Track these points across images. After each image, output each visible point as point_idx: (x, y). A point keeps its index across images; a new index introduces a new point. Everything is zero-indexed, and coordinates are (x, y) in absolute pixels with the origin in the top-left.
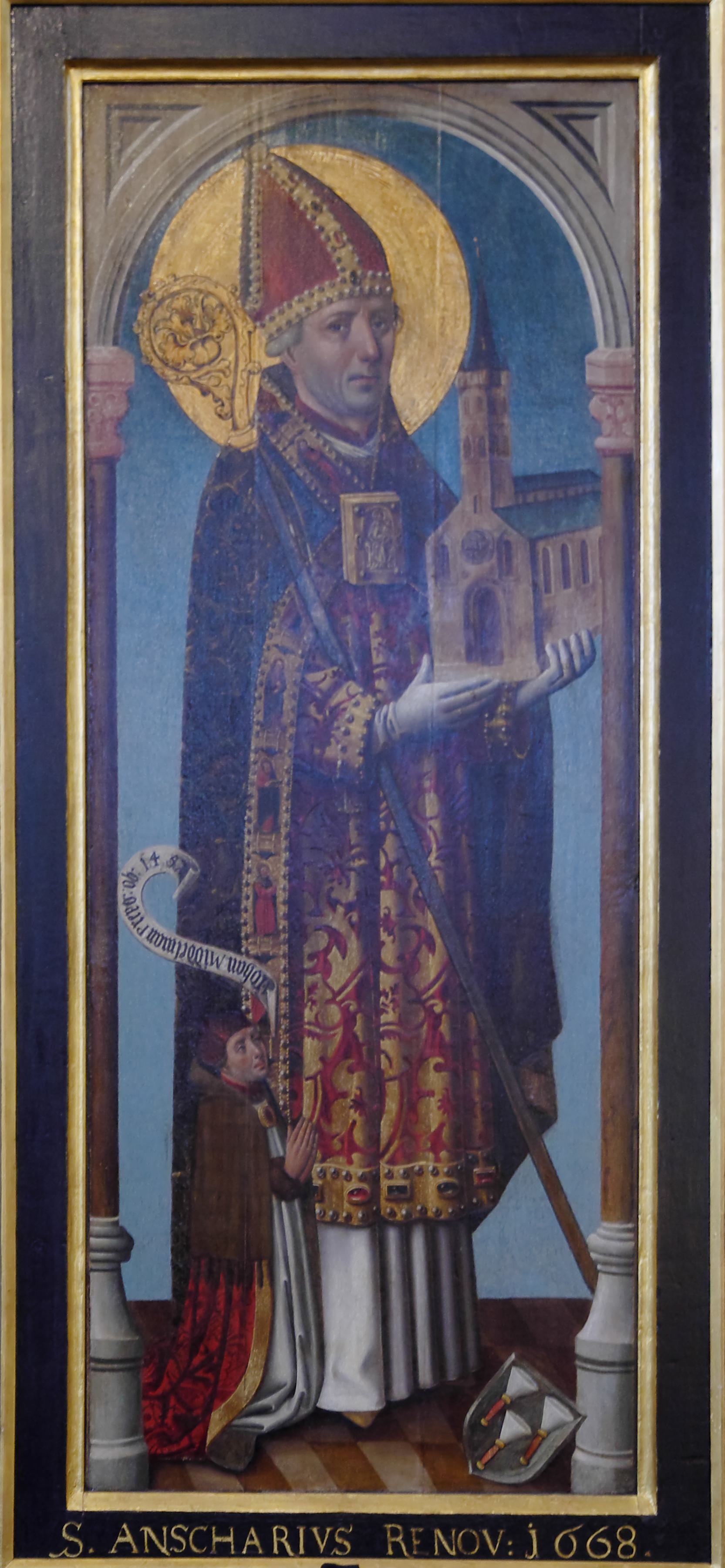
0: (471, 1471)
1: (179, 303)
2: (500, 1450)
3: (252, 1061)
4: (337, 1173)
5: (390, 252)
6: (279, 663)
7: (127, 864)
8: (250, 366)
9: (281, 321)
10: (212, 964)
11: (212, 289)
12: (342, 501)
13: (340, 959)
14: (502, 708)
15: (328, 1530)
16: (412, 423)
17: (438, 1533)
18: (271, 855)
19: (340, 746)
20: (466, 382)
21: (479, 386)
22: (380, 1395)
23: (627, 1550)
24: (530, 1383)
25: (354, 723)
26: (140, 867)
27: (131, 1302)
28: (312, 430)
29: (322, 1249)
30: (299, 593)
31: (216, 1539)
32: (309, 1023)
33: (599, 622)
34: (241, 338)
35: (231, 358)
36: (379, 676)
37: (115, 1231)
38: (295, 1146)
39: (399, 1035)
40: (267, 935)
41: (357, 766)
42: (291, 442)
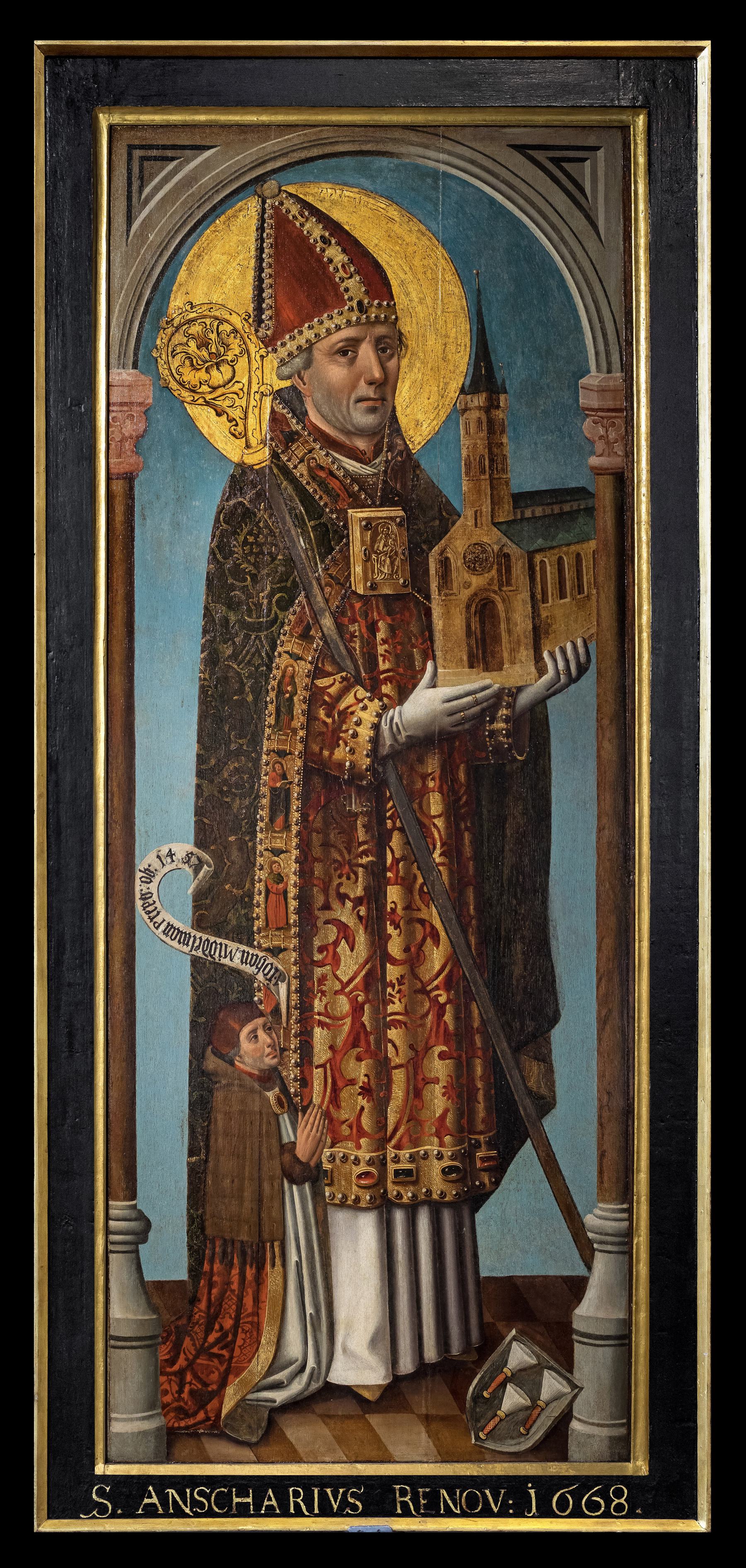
0: (473, 1441)
1: (196, 329)
2: (501, 1420)
3: (264, 1050)
4: (345, 1158)
5: (394, 283)
6: (291, 669)
7: (145, 859)
8: (262, 389)
9: (291, 346)
10: (226, 957)
11: (227, 316)
12: (349, 515)
13: (348, 952)
14: (503, 712)
15: (341, 1490)
16: (416, 443)
17: (443, 1492)
18: (283, 852)
19: (348, 749)
20: (466, 404)
21: (479, 408)
22: (387, 1370)
23: (620, 1507)
24: (530, 1357)
25: (361, 726)
26: (156, 864)
27: (148, 1282)
28: (321, 449)
29: (332, 1230)
30: (309, 603)
31: (236, 1500)
32: (319, 1014)
33: (593, 630)
34: (254, 362)
35: (245, 380)
37: (134, 1214)
38: (306, 1132)
39: (405, 1024)
40: (278, 929)
41: (364, 767)
42: (302, 461)
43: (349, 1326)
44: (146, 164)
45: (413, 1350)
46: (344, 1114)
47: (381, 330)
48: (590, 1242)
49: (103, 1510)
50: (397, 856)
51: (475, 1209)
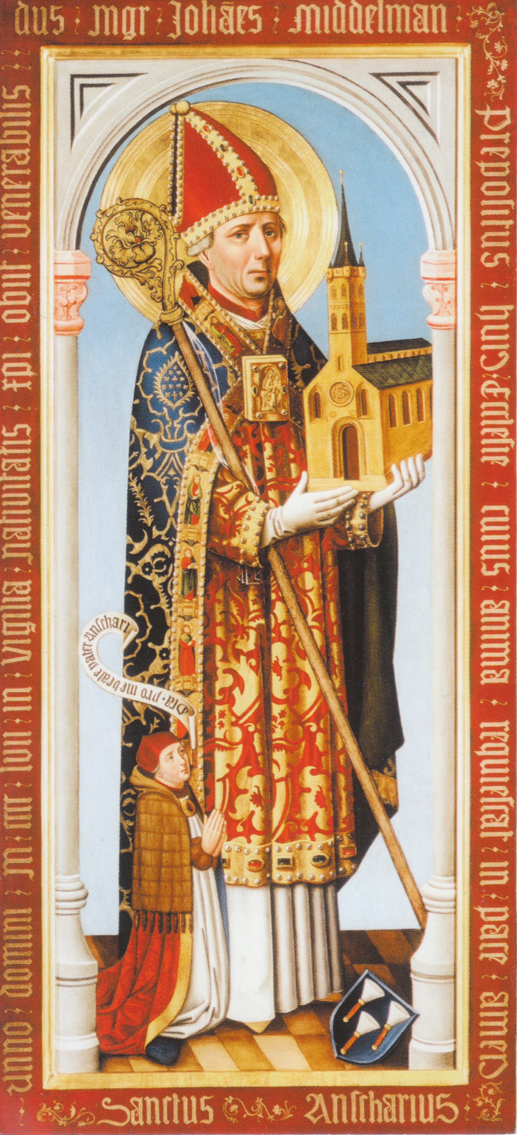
36: (270, 488)
44: (85, 90)
46: (237, 816)
50: (280, 621)
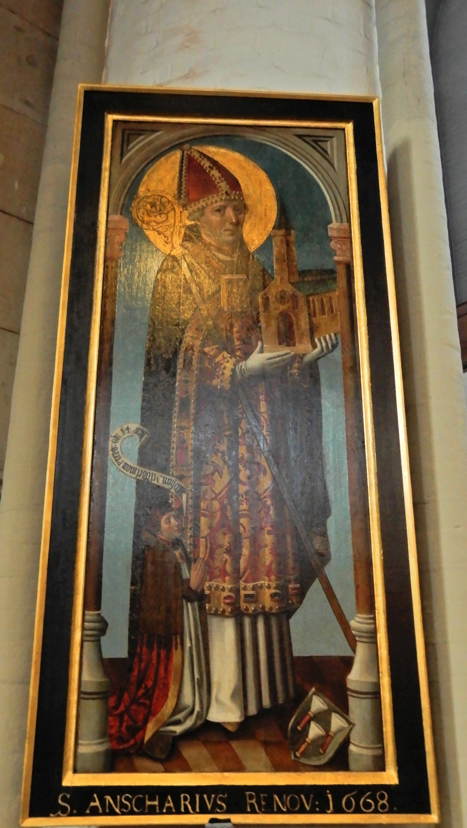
0: (293, 758)
1: (150, 200)
4: (217, 588)
7: (115, 431)
9: (195, 208)
10: (154, 480)
11: (165, 195)
14: (296, 365)
17: (276, 797)
23: (383, 806)
25: (226, 370)
27: (105, 659)
32: (204, 510)
35: (173, 221)
43: (219, 685)
45: (256, 699)
47: (235, 203)
48: (354, 636)
49: (64, 810)
51: (289, 617)
